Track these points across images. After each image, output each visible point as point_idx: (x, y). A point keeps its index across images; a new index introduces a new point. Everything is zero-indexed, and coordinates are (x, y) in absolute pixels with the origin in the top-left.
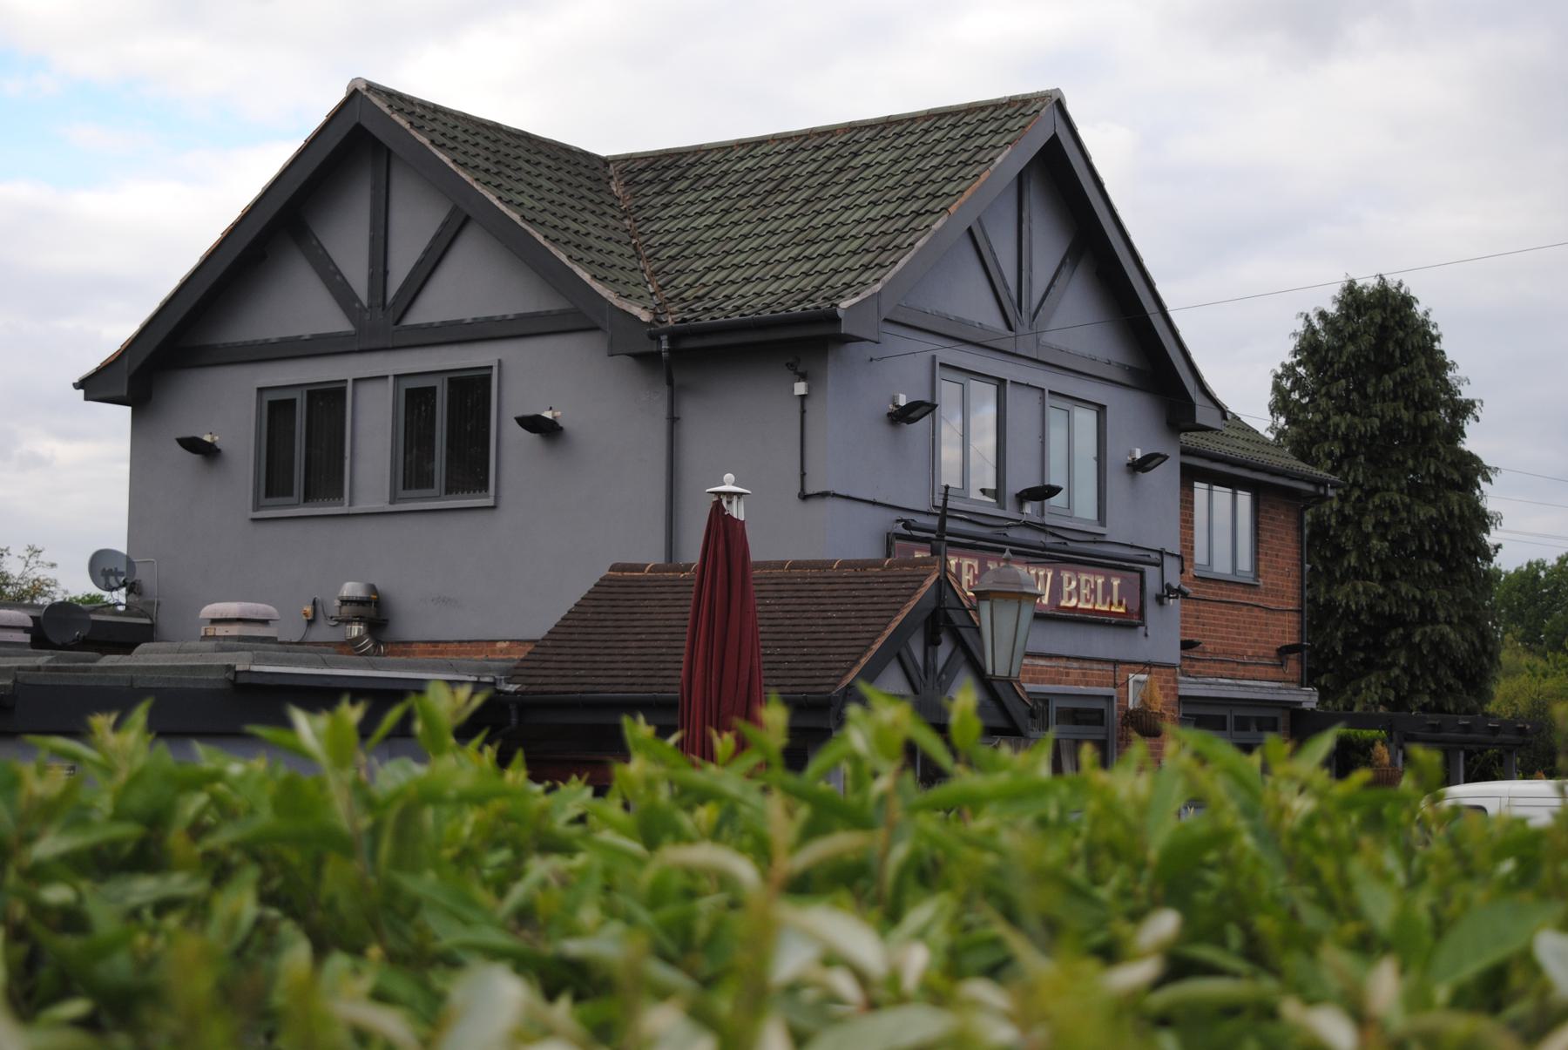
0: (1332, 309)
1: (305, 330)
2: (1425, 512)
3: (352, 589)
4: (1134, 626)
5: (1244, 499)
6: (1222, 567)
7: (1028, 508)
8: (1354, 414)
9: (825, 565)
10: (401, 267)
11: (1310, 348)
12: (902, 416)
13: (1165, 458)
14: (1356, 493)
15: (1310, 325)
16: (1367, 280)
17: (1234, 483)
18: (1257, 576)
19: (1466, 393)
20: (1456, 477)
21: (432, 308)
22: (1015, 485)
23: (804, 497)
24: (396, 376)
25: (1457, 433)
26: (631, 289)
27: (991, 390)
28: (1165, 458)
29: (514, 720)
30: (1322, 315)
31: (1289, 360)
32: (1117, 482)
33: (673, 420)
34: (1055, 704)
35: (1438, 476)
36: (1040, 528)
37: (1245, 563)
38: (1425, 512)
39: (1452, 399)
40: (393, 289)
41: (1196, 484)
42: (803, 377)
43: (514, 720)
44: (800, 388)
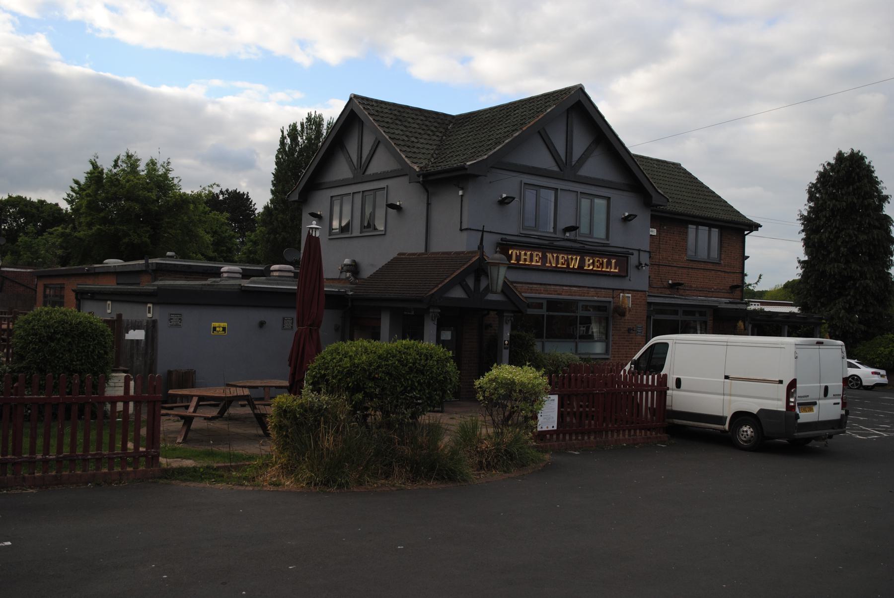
0: (833, 162)
1: (341, 177)
2: (863, 237)
3: (347, 261)
4: (624, 277)
5: (715, 232)
6: (703, 255)
7: (568, 234)
8: (837, 200)
9: (449, 253)
10: (561, 150)
11: (823, 177)
12: (503, 202)
13: (636, 216)
14: (835, 231)
15: (825, 169)
16: (847, 151)
17: (711, 226)
18: (720, 260)
19: (885, 193)
20: (877, 224)
21: (373, 169)
22: (562, 225)
23: (461, 230)
24: (363, 192)
25: (881, 208)
26: (415, 160)
27: (552, 193)
28: (636, 216)
29: (350, 304)
30: (829, 164)
31: (814, 182)
32: (616, 226)
33: (428, 204)
34: (580, 304)
35: (869, 224)
36: (575, 241)
37: (715, 254)
38: (863, 237)
39: (879, 195)
40: (355, 163)
41: (690, 226)
42: (462, 189)
43: (350, 304)
44: (461, 193)
